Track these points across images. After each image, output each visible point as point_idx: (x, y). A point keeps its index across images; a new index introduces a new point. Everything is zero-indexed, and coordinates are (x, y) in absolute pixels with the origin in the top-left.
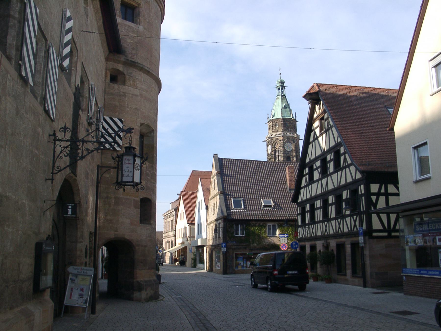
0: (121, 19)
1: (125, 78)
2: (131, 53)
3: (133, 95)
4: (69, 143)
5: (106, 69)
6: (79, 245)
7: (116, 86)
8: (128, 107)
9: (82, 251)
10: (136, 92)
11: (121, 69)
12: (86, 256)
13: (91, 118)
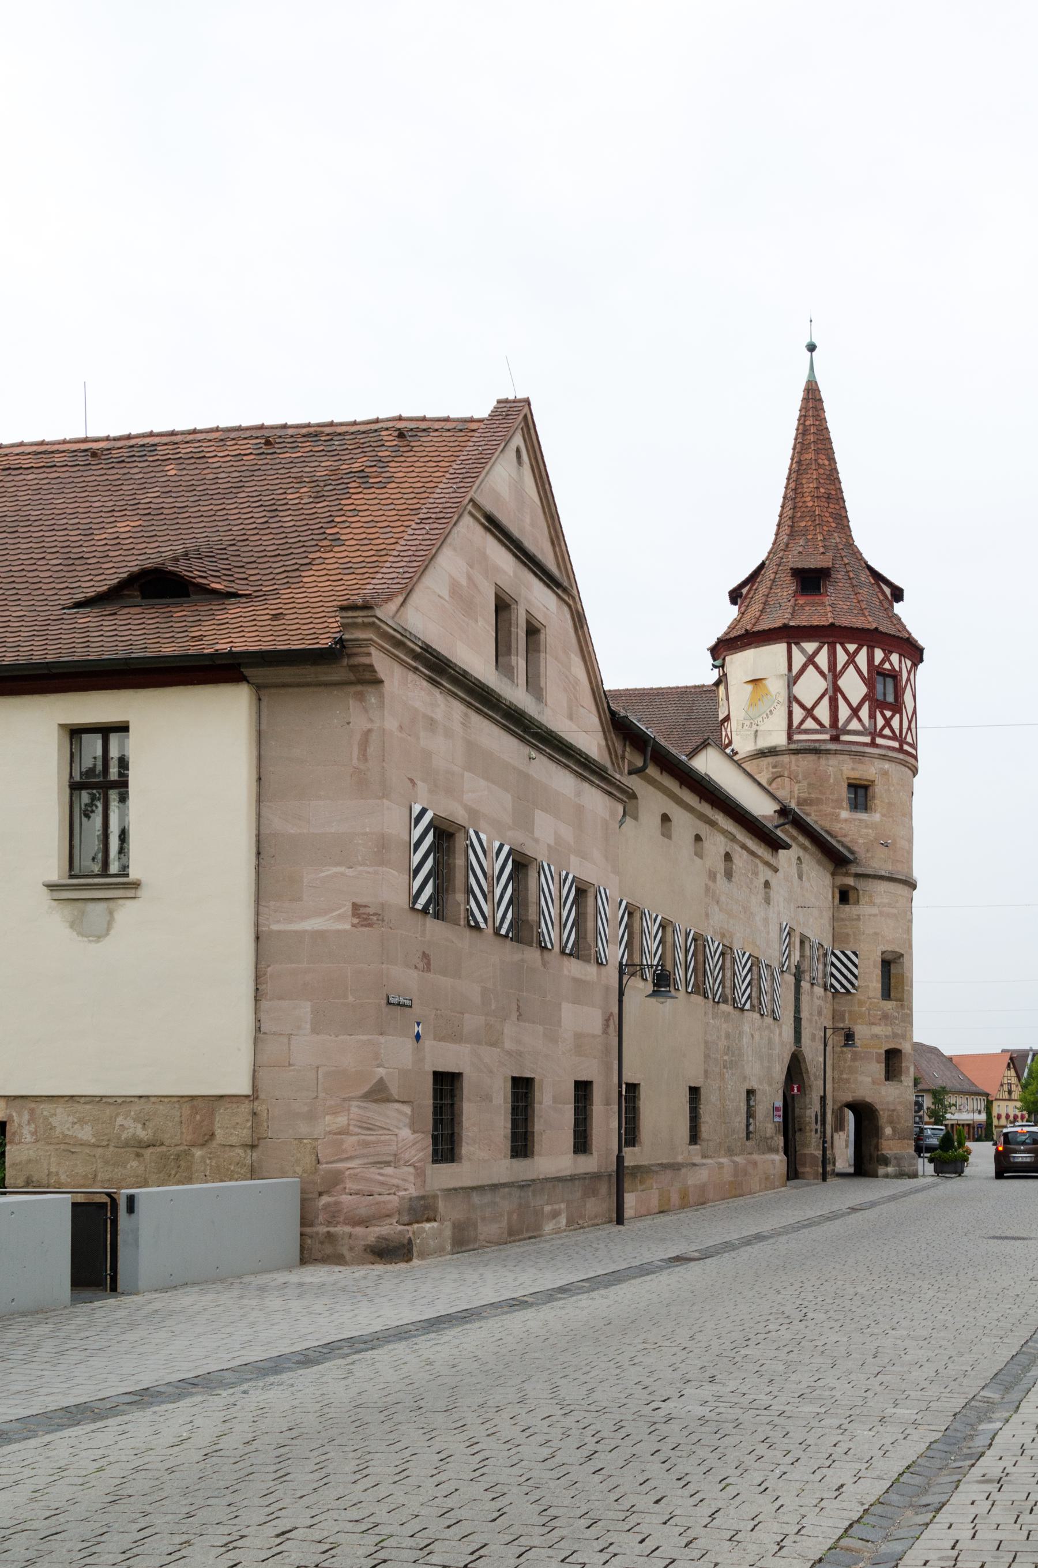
3: (870, 915)
5: (833, 887)
6: (808, 1112)
7: (847, 908)
9: (811, 1118)
10: (875, 911)
12: (816, 1123)
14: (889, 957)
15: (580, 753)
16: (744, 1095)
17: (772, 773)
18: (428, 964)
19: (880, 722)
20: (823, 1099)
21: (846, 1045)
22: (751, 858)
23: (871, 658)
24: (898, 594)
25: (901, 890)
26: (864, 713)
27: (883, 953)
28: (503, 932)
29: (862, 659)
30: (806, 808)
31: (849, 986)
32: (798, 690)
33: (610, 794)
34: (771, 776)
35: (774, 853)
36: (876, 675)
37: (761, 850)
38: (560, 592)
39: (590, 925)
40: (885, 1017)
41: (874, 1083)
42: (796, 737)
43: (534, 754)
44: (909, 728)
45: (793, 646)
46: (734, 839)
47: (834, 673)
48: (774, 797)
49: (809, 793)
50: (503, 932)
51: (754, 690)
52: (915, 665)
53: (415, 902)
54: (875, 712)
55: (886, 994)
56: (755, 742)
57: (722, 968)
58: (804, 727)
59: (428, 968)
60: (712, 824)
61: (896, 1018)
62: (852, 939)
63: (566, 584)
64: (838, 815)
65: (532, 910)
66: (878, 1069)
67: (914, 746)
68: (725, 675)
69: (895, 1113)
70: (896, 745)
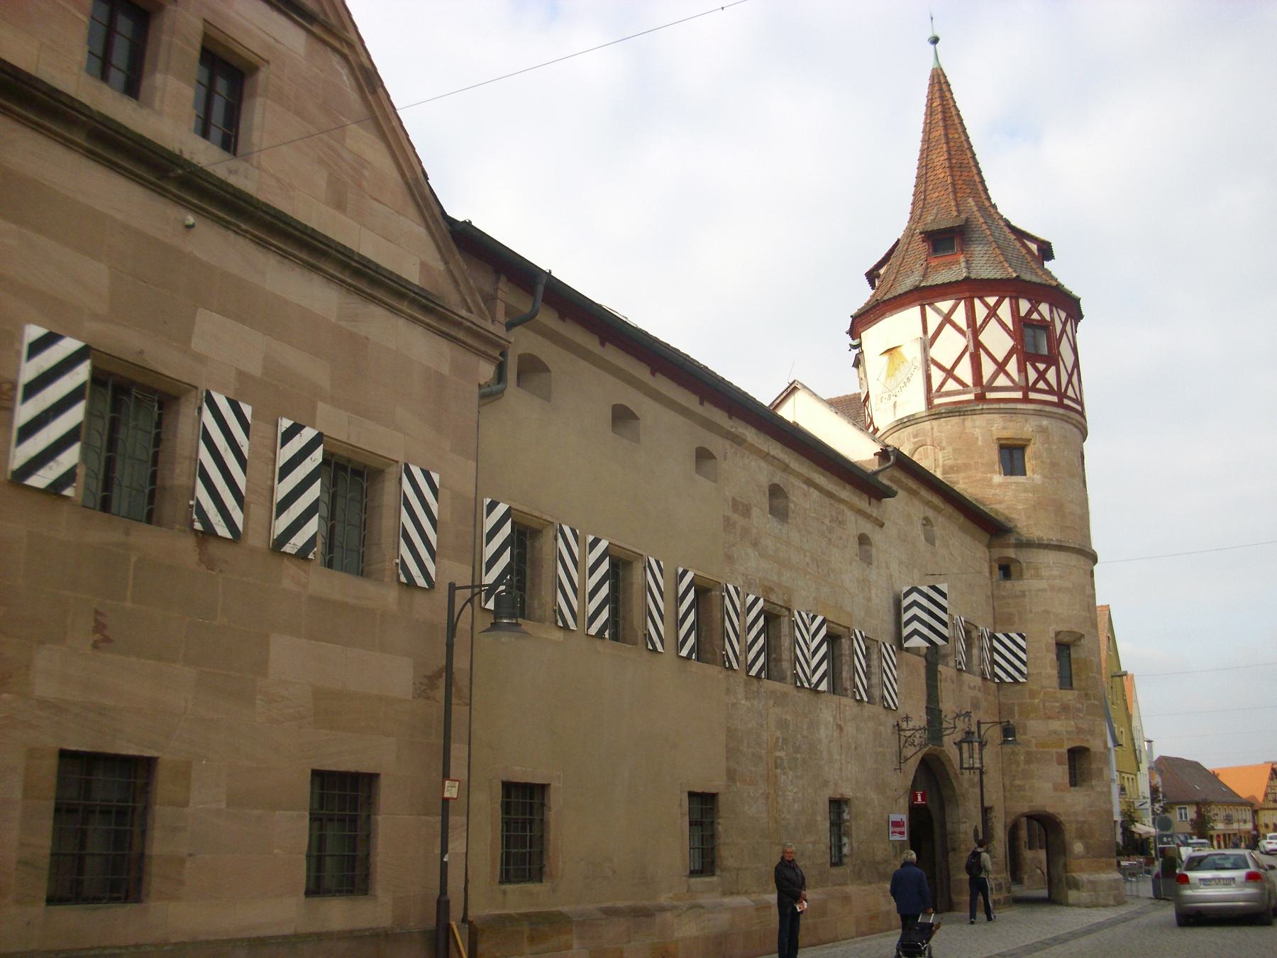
0: (1003, 475)
1: (1021, 570)
2: (1027, 525)
4: (977, 302)
5: (990, 561)
6: (963, 827)
7: (1008, 584)
8: (1031, 612)
10: (1043, 584)
11: (1013, 556)
13: (960, 663)
14: (1066, 639)
17: (914, 443)
19: (1032, 376)
20: (986, 811)
21: (1005, 742)
22: (827, 500)
23: (1015, 310)
26: (1012, 367)
27: (1058, 634)
29: (1005, 311)
30: (953, 475)
31: (1016, 675)
32: (935, 352)
34: (912, 446)
35: (873, 501)
36: (1023, 329)
37: (861, 502)
38: (316, 29)
40: (1065, 709)
41: (1056, 788)
42: (937, 401)
44: (1070, 382)
46: (786, 468)
47: (975, 329)
49: (955, 460)
51: (891, 361)
54: (1026, 365)
55: (1066, 680)
56: (895, 414)
61: (1079, 710)
62: (1016, 619)
63: (333, 20)
64: (991, 479)
66: (1061, 772)
68: (862, 352)
69: (1086, 826)
70: (1055, 399)
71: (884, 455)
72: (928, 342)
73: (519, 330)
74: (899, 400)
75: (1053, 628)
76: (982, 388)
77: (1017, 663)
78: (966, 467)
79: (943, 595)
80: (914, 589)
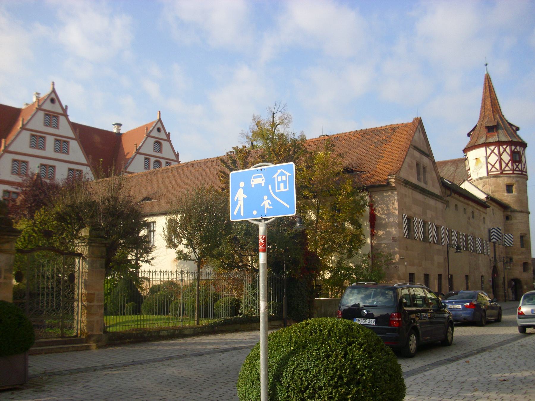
4: (501, 147)
5: (504, 215)
7: (508, 221)
10: (517, 221)
14: (522, 235)
15: (436, 194)
16: (465, 277)
18: (407, 249)
19: (515, 167)
20: (504, 278)
23: (511, 149)
24: (518, 129)
25: (525, 215)
26: (510, 165)
27: (520, 234)
28: (421, 240)
29: (508, 150)
33: (443, 203)
37: (482, 209)
39: (440, 236)
40: (522, 253)
43: (426, 197)
44: (524, 167)
45: (487, 148)
47: (500, 155)
48: (485, 193)
50: (421, 240)
52: (525, 149)
53: (404, 236)
55: (522, 245)
57: (473, 243)
58: (492, 170)
59: (407, 250)
60: (468, 204)
65: (427, 234)
66: (521, 269)
67: (526, 172)
70: (520, 172)
71: (487, 198)
72: (487, 158)
73: (448, 197)
74: (479, 172)
75: (520, 232)
76: (502, 170)
77: (511, 241)
78: (498, 191)
79: (500, 230)
80: (493, 228)
